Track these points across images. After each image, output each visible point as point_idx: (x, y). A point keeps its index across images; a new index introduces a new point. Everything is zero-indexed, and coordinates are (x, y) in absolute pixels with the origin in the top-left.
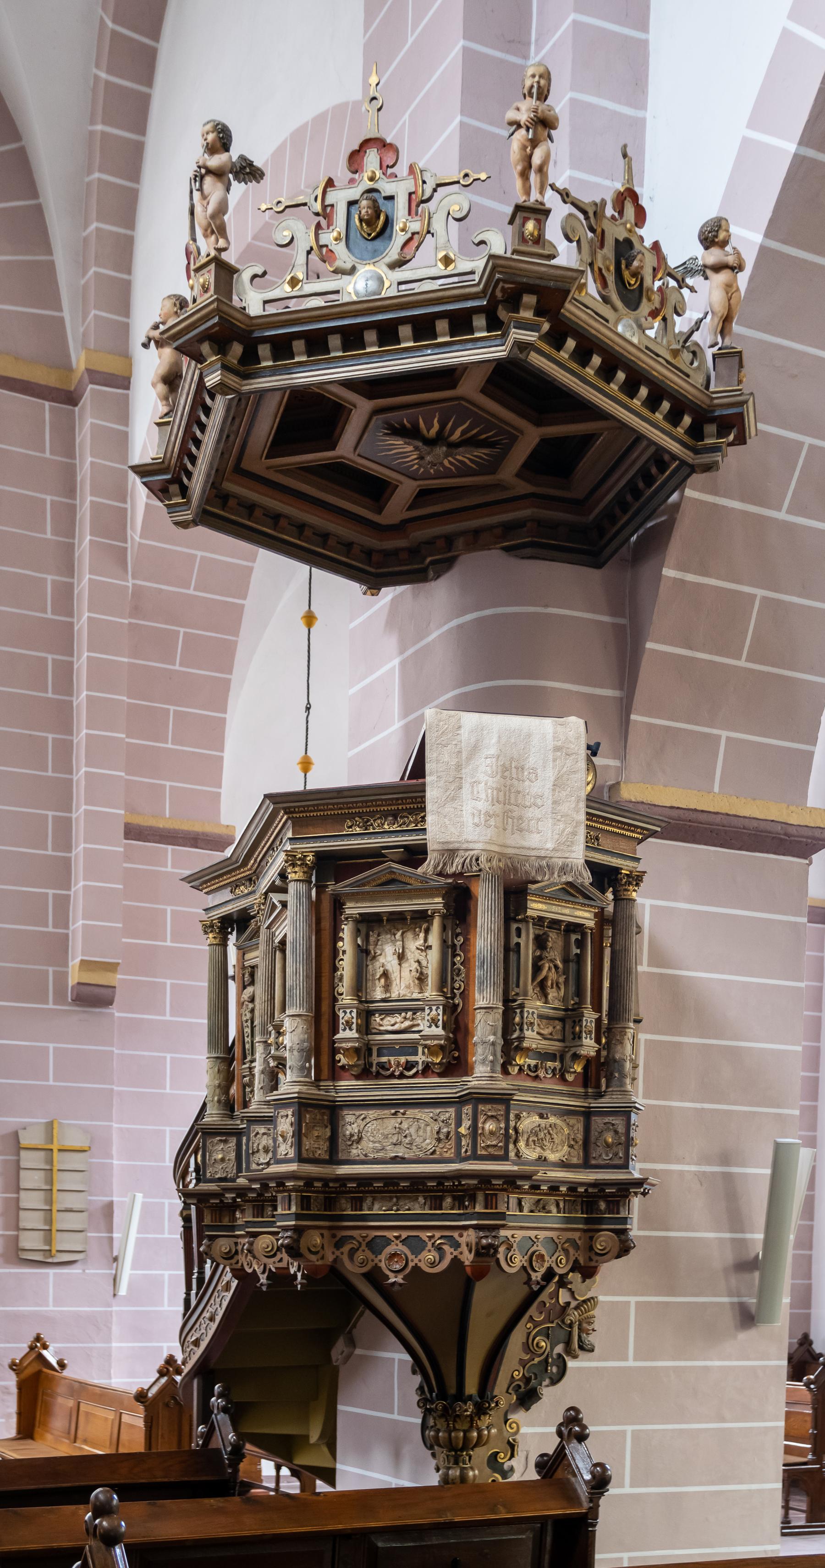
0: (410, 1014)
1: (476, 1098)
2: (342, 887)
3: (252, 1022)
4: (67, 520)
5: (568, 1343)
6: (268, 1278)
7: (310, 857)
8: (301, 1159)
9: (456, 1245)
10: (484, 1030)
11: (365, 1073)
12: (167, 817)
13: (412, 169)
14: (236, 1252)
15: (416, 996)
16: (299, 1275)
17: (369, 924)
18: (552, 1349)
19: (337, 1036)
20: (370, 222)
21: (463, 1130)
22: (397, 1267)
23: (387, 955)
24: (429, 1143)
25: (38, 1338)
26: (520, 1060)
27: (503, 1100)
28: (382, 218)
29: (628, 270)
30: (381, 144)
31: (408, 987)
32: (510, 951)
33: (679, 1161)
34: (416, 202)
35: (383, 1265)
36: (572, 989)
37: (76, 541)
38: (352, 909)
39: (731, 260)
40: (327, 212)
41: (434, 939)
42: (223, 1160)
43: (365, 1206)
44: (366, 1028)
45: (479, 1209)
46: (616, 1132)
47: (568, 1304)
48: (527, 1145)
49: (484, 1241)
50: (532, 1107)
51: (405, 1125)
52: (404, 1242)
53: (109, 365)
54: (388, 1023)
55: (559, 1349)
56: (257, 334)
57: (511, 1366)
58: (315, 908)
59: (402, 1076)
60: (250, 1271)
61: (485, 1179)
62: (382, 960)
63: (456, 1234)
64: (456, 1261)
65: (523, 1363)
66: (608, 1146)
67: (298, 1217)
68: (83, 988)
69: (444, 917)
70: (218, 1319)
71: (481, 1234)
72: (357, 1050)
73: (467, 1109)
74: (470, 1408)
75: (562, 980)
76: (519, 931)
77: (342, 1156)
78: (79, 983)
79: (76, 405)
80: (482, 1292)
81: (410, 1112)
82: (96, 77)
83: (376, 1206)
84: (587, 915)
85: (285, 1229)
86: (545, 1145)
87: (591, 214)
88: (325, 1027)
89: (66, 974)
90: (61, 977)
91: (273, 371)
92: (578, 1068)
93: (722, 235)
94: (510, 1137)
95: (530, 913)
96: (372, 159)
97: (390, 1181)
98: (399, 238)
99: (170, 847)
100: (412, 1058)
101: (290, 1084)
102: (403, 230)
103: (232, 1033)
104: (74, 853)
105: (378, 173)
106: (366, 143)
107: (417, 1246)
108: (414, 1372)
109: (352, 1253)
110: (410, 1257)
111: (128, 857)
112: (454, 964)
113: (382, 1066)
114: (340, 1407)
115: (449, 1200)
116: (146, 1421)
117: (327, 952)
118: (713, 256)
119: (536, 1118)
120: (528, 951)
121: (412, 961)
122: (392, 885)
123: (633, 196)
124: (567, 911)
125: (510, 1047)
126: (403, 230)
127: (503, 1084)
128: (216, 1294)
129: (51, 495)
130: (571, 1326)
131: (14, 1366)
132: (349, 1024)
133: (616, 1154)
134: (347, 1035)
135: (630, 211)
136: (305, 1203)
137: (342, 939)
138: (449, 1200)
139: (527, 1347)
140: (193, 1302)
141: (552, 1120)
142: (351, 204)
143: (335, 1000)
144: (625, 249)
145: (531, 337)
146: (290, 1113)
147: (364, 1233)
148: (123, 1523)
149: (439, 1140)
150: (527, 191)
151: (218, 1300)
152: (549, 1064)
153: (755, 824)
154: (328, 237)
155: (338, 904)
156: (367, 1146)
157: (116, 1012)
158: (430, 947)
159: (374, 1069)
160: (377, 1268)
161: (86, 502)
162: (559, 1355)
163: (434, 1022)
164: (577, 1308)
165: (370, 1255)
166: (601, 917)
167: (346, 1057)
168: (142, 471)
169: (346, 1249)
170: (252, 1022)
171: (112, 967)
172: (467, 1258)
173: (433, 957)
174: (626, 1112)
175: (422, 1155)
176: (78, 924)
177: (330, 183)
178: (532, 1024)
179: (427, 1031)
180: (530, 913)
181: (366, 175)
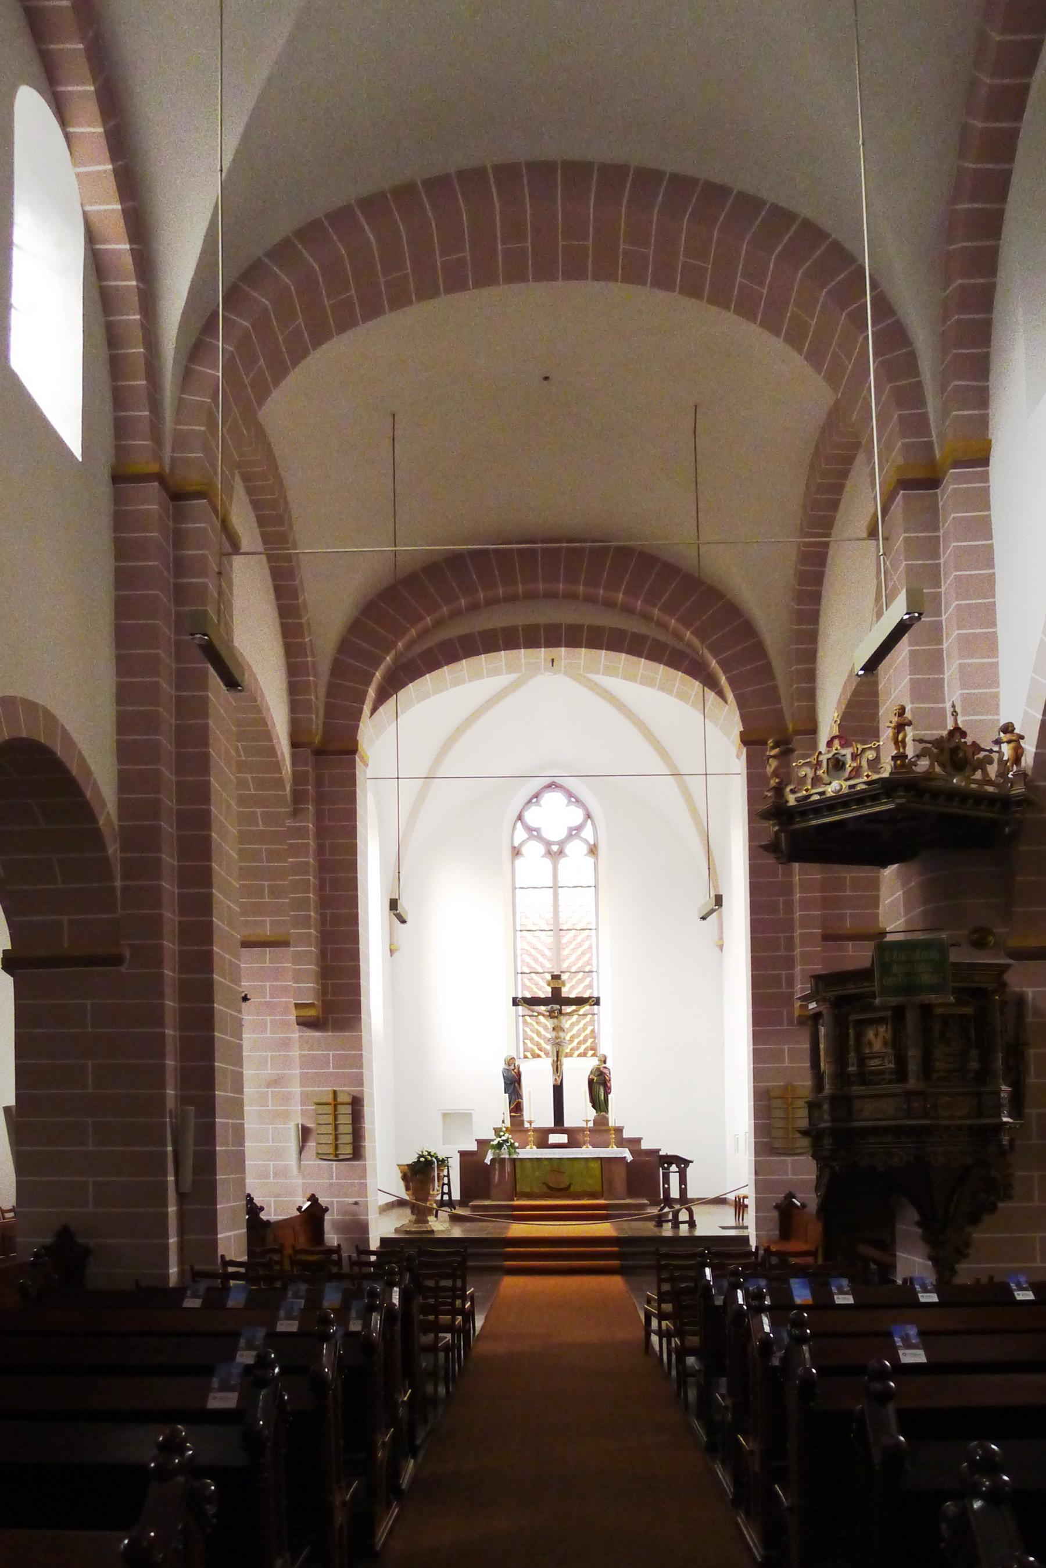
1: (909, 1095)
10: (913, 1065)
11: (863, 1083)
23: (870, 1034)
90: (790, 1014)
118: (1008, 736)
125: (927, 1069)
132: (853, 1065)
145: (903, 801)
154: (820, 772)
163: (890, 1062)
173: (889, 1036)
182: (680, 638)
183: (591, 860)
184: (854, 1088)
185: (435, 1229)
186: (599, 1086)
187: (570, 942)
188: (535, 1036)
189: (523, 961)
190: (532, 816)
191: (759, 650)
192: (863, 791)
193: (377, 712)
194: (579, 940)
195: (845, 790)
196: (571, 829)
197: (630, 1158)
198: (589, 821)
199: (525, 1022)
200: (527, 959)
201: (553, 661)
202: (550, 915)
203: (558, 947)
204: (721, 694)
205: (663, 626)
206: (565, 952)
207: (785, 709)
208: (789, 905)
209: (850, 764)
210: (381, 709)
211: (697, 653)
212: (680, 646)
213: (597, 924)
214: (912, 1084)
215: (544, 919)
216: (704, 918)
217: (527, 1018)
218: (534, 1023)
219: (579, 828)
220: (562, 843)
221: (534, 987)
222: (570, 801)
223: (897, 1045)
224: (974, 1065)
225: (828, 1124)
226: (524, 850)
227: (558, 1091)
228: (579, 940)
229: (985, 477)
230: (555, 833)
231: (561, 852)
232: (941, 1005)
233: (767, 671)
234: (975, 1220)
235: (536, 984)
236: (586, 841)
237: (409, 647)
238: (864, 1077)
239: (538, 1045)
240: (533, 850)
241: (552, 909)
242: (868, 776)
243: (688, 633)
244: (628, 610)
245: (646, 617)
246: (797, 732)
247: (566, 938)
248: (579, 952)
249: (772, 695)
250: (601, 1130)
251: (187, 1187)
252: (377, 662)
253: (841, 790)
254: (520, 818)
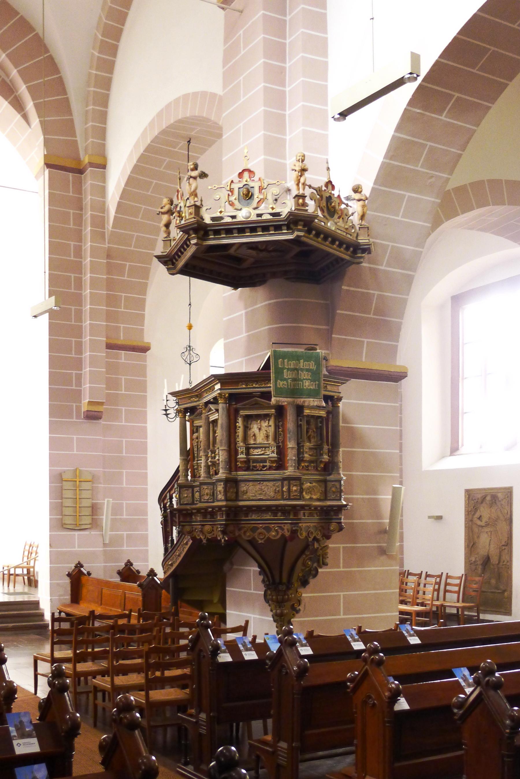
0: (263, 449)
1: (289, 479)
2: (239, 406)
3: (197, 447)
4: (79, 220)
5: (318, 562)
6: (207, 541)
7: (227, 395)
8: (226, 500)
9: (283, 529)
10: (291, 455)
11: (248, 469)
12: (122, 339)
13: (260, 179)
14: (193, 531)
15: (266, 442)
16: (223, 540)
17: (248, 419)
18: (313, 565)
19: (239, 457)
20: (247, 195)
21: (284, 489)
22: (262, 537)
23: (255, 428)
24: (272, 494)
25: (79, 563)
27: (298, 479)
28: (250, 194)
29: (329, 204)
30: (249, 171)
31: (263, 439)
32: (299, 427)
33: (357, 494)
34: (261, 189)
35: (256, 537)
36: (319, 438)
37: (83, 228)
39: (363, 198)
40: (231, 190)
41: (272, 423)
42: (187, 496)
43: (249, 516)
45: (291, 517)
46: (336, 488)
47: (318, 548)
48: (306, 493)
49: (294, 528)
50: (307, 481)
51: (263, 488)
52: (264, 528)
53: (98, 161)
54: (256, 452)
56: (209, 229)
57: (298, 572)
59: (261, 470)
60: (198, 538)
61: (294, 506)
62: (253, 430)
63: (282, 525)
64: (283, 535)
65: (302, 570)
66: (334, 492)
67: (226, 520)
68: (89, 413)
69: (275, 417)
71: (293, 526)
72: (245, 462)
73: (286, 483)
74: (284, 588)
75: (315, 435)
77: (240, 498)
78: (87, 411)
79: (82, 174)
80: (290, 546)
81: (265, 483)
82: (93, 54)
83: (253, 516)
84: (324, 413)
87: (319, 190)
88: (233, 453)
89: (80, 407)
90: (79, 408)
91: (214, 239)
92: (322, 466)
93: (360, 190)
94: (301, 491)
95: (305, 414)
96: (246, 174)
98: (256, 200)
99: (123, 352)
100: (265, 464)
101: (222, 474)
102: (257, 198)
104: (84, 356)
105: (248, 180)
106: (244, 170)
107: (268, 529)
108: (260, 574)
109: (245, 533)
110: (266, 534)
111: (107, 357)
112: (279, 431)
113: (255, 467)
114: (227, 588)
115: (280, 514)
116: (143, 597)
117: (232, 427)
118: (357, 196)
119: (309, 484)
120: (305, 427)
121: (264, 430)
122: (256, 406)
123: (330, 182)
124: (317, 412)
125: (300, 460)
126: (257, 198)
127: (298, 474)
128: (181, 546)
129: (72, 210)
130: (319, 556)
131: (69, 575)
132: (242, 453)
133: (336, 496)
134: (242, 456)
135: (330, 187)
136: (228, 515)
137: (238, 423)
138: (280, 514)
139: (304, 564)
141: (314, 484)
143: (236, 444)
144: (329, 199)
145: (301, 234)
146: (222, 484)
147: (249, 525)
149: (275, 493)
150: (299, 189)
151: (182, 549)
152: (312, 464)
153: (378, 372)
154: (232, 198)
155: (237, 411)
156: (250, 495)
158: (270, 426)
159: (251, 468)
160: (254, 538)
161: (88, 214)
162: (315, 567)
163: (273, 452)
164: (321, 550)
165: (252, 533)
166: (328, 413)
168: (158, 257)
169: (242, 531)
170: (197, 447)
171: (102, 404)
172: (287, 534)
175: (269, 498)
176: (86, 386)
177: (232, 182)
178: (307, 452)
179: (271, 455)
180: (305, 414)
181: (245, 180)
191: (60, 86)
195: (253, 218)
207: (79, 142)
208: (79, 315)
211: (8, 75)
214: (290, 471)
216: (35, 316)
234: (305, 583)
238: (249, 465)
246: (92, 165)
249: (69, 127)
253: (249, 217)
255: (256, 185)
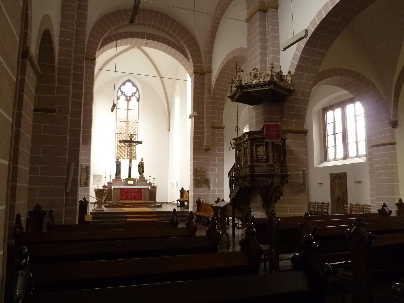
1: (271, 165)
4: (203, 89)
9: (268, 182)
10: (271, 158)
12: (216, 125)
17: (257, 146)
21: (269, 169)
23: (259, 149)
25: (199, 198)
26: (275, 161)
32: (273, 148)
38: (255, 144)
40: (251, 75)
41: (264, 147)
44: (257, 157)
54: (259, 157)
55: (279, 195)
58: (251, 144)
61: (272, 174)
70: (236, 193)
73: (269, 167)
76: (274, 146)
85: (248, 181)
86: (278, 171)
87: (278, 73)
92: (281, 161)
96: (255, 70)
97: (261, 175)
98: (258, 77)
103: (238, 156)
118: (289, 75)
123: (281, 71)
125: (274, 159)
132: (255, 157)
134: (255, 158)
140: (232, 191)
142: (253, 74)
145: (273, 87)
148: (226, 218)
157: (210, 152)
158: (264, 148)
161: (206, 87)
163: (265, 157)
167: (254, 160)
168: (228, 97)
173: (264, 150)
174: (287, 166)
177: (251, 72)
182: (179, 43)
183: (137, 103)
184: (255, 164)
185: (104, 209)
186: (141, 167)
187: (131, 126)
188: (120, 152)
189: (118, 130)
190: (123, 88)
191: (198, 49)
192: (262, 83)
193: (100, 50)
194: (133, 125)
195: (257, 82)
196: (133, 93)
197: (150, 188)
198: (138, 92)
199: (117, 148)
200: (119, 130)
201: (147, 43)
202: (126, 117)
203: (127, 127)
204: (188, 59)
205: (175, 38)
206: (129, 128)
209: (259, 76)
210: (101, 49)
212: (179, 45)
213: (138, 121)
214: (271, 163)
215: (124, 119)
217: (118, 147)
218: (120, 149)
219: (135, 93)
220: (130, 97)
221: (120, 138)
222: (133, 85)
223: (267, 151)
224: (282, 159)
225: (249, 173)
226: (120, 98)
227: (130, 168)
228: (133, 125)
229: (277, 12)
230: (129, 94)
231: (130, 100)
232: (277, 142)
233: (200, 55)
234: (276, 202)
235: (121, 137)
236: (136, 97)
237: (111, 32)
238: (257, 161)
239: (121, 155)
240: (123, 98)
241: (126, 116)
242: (263, 80)
243: (182, 42)
244: (167, 33)
245: (172, 36)
247: (130, 124)
248: (133, 128)
249: (201, 62)
250: (142, 180)
251: (68, 191)
252: (103, 35)
254: (120, 88)
255: (258, 73)
